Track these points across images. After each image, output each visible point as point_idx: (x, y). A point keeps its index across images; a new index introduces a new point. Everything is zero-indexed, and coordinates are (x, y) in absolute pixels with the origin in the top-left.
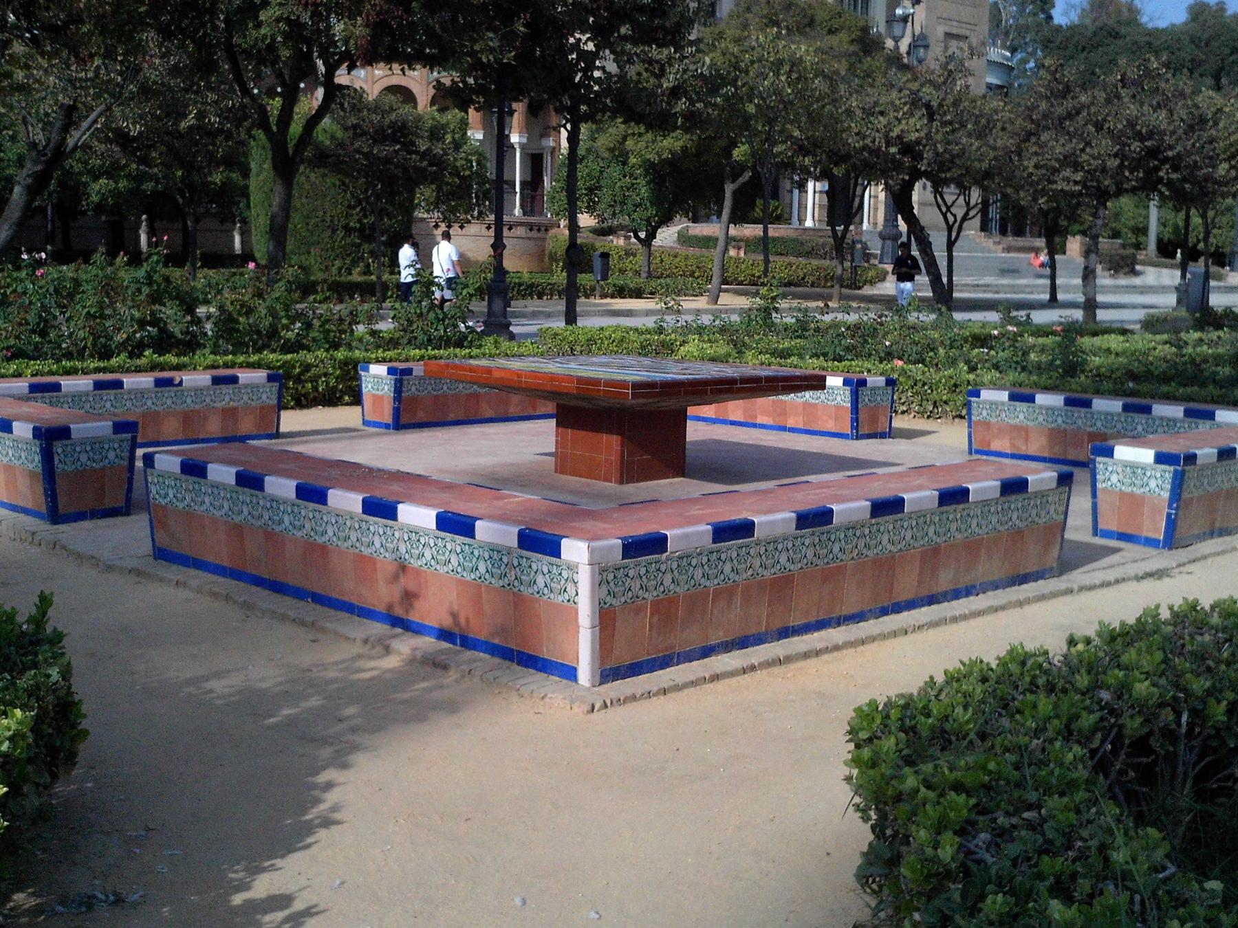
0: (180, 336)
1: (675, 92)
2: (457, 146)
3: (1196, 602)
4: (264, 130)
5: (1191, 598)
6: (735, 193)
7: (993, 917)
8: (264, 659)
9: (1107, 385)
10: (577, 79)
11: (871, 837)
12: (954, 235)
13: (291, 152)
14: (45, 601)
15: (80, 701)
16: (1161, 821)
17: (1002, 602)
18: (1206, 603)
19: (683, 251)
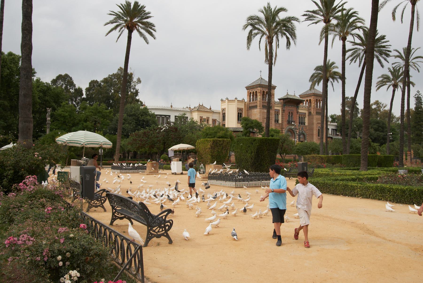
0: (126, 107)
1: (52, 99)
2: (185, 123)
3: (40, 79)
4: (278, 13)
5: (124, 3)
6: (82, 95)
7: (53, 266)
8: (117, 96)
9: (88, 177)
10: (246, 172)
11: (347, 37)
12: (165, 214)
13: (400, 74)
14: (268, 4)
15: (126, 2)
16: (126, 275)
17: (78, 144)
18: (415, 103)
19: (129, 118)
